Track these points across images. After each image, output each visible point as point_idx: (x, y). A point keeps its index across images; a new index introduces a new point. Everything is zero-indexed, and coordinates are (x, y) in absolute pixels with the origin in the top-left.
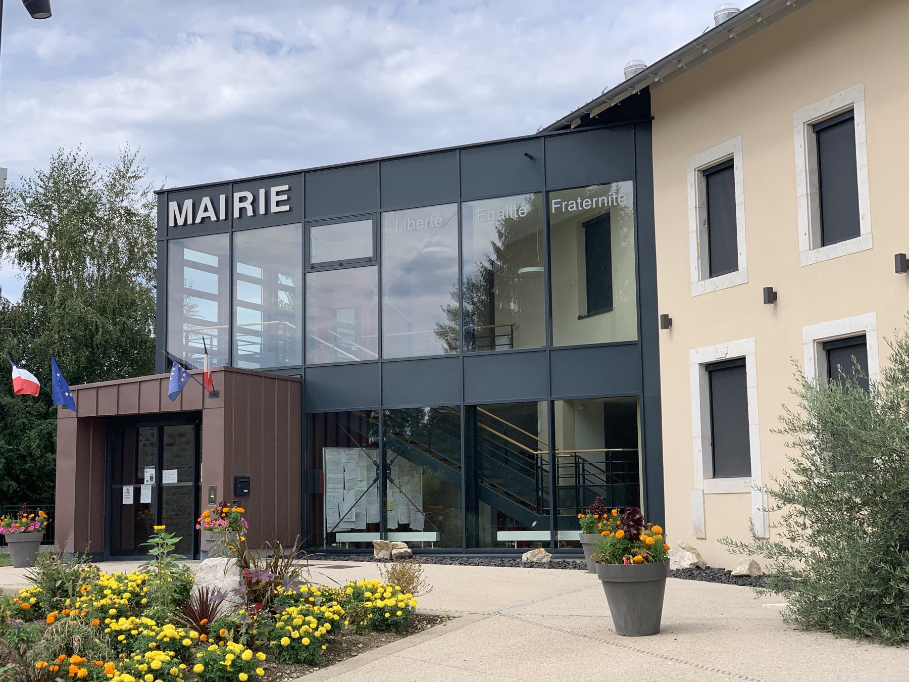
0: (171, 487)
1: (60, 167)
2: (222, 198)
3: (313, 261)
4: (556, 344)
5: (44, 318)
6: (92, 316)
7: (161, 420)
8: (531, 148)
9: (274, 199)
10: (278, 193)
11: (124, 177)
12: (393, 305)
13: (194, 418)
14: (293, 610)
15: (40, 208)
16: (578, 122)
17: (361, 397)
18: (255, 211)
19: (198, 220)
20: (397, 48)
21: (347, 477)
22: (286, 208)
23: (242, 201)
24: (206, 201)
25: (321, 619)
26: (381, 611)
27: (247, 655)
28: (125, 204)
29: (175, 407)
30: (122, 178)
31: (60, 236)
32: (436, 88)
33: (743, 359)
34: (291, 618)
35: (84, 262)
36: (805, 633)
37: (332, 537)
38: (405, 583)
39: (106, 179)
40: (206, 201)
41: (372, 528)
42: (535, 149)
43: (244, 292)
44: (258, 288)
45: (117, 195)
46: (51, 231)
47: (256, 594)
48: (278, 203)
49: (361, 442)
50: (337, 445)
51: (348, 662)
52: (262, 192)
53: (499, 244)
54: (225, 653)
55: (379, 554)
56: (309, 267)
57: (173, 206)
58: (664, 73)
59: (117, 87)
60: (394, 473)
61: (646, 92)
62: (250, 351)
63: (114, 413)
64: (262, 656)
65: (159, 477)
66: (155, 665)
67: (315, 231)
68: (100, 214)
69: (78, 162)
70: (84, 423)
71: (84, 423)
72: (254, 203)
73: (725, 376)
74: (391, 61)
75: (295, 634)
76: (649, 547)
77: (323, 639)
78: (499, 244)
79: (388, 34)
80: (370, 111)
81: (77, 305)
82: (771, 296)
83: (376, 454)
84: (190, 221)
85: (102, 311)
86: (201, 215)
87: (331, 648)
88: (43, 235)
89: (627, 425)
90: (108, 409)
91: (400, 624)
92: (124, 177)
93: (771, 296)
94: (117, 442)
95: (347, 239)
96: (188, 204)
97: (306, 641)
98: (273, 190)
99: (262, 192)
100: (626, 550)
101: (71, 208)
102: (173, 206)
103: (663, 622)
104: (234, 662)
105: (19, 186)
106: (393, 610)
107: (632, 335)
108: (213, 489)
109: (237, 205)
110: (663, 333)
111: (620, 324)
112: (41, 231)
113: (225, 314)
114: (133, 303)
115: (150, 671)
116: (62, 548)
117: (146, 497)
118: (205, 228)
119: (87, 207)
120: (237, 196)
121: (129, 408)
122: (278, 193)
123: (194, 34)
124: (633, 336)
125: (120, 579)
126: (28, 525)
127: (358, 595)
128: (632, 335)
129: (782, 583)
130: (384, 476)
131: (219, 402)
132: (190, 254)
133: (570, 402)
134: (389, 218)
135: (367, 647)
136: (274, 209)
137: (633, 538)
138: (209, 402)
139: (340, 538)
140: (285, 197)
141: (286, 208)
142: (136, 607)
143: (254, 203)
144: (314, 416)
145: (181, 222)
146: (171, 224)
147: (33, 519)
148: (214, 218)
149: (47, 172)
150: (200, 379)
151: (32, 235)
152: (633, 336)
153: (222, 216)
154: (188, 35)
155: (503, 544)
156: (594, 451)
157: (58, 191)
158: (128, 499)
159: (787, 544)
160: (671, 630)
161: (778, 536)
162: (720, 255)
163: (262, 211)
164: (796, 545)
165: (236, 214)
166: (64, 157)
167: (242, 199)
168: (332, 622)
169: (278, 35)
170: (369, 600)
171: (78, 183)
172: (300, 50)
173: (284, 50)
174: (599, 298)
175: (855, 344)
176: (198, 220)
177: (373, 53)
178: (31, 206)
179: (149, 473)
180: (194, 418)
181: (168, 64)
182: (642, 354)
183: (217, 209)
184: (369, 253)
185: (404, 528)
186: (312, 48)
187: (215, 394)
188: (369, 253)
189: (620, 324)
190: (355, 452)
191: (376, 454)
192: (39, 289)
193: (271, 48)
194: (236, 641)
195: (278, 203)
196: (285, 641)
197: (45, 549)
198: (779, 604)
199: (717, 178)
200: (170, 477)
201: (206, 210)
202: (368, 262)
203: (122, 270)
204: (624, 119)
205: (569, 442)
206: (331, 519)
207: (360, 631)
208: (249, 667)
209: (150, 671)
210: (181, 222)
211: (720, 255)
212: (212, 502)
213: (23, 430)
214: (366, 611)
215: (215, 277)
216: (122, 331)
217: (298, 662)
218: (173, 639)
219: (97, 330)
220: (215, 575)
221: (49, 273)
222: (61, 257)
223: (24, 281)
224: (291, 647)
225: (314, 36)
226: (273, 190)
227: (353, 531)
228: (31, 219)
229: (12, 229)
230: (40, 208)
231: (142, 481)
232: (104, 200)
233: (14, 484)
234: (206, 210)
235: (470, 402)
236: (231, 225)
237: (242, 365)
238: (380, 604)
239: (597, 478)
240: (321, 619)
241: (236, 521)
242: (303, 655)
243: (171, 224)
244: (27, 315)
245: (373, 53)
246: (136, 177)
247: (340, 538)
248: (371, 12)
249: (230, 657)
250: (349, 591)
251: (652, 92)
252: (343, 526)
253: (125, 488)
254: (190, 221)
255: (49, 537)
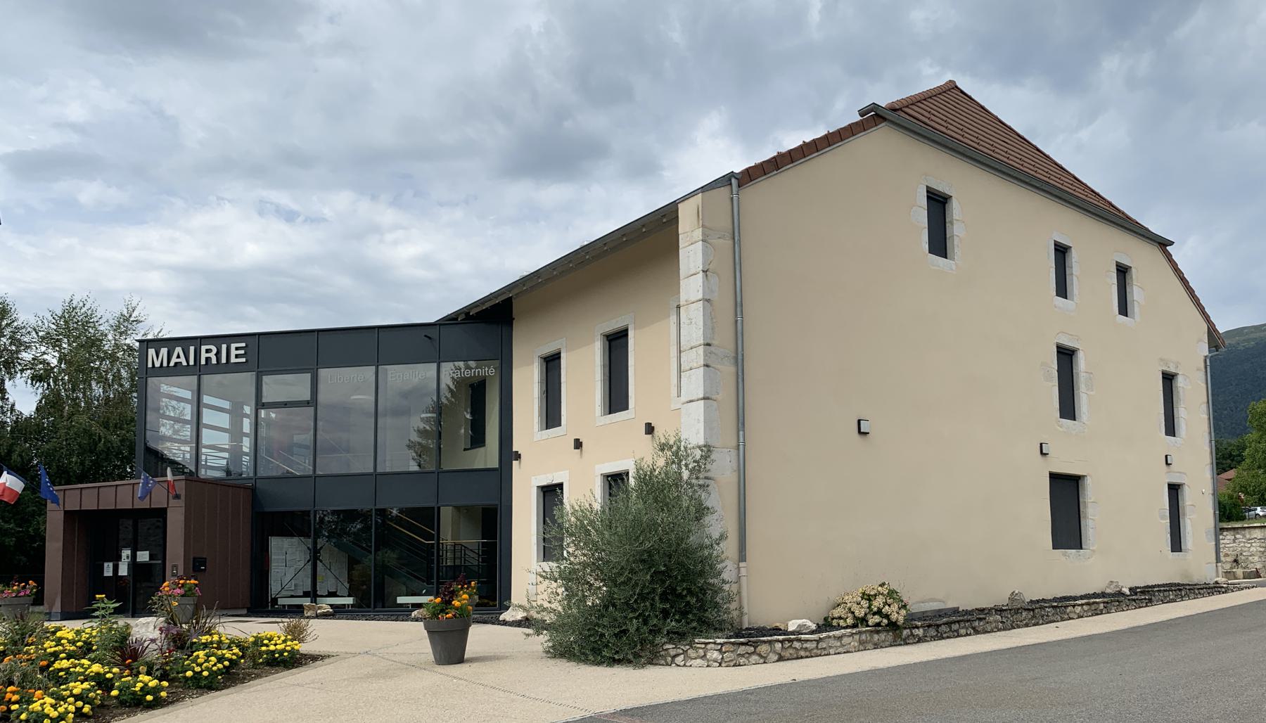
0: (144, 565)
1: (70, 310)
2: (192, 349)
3: (264, 400)
4: (445, 468)
5: (55, 427)
6: (96, 429)
7: (136, 515)
8: (429, 332)
10: (237, 349)
11: (127, 320)
13: (161, 514)
14: (201, 653)
15: (50, 340)
16: (463, 316)
17: (296, 501)
18: (218, 359)
19: (172, 364)
21: (287, 559)
22: (244, 360)
23: (208, 353)
24: (179, 350)
26: (273, 652)
27: (154, 683)
28: (128, 341)
30: (125, 323)
31: (69, 363)
32: (426, 261)
34: (198, 657)
36: (552, 662)
37: (275, 601)
38: (296, 634)
39: (111, 322)
40: (179, 350)
41: (306, 594)
42: (433, 333)
43: (208, 417)
44: (227, 416)
45: (121, 334)
46: (60, 361)
47: (180, 643)
48: (237, 356)
49: (302, 533)
51: (240, 686)
52: (224, 347)
53: (452, 387)
54: (135, 683)
56: (260, 405)
57: (152, 352)
60: (324, 555)
61: (509, 300)
62: (214, 462)
65: (134, 556)
67: (266, 379)
69: (87, 306)
72: (218, 354)
73: (551, 493)
74: (389, 237)
75: (198, 669)
76: (457, 609)
77: (219, 672)
78: (452, 387)
79: (388, 216)
80: (373, 275)
82: (578, 444)
84: (165, 364)
85: (106, 425)
86: (174, 360)
87: (229, 676)
88: (54, 362)
89: (494, 522)
90: (90, 504)
91: (293, 661)
92: (127, 320)
93: (578, 444)
96: (164, 351)
97: (205, 673)
98: (233, 346)
99: (224, 347)
100: (442, 611)
102: (152, 352)
104: (142, 689)
105: (33, 321)
106: (281, 652)
107: (494, 463)
108: (175, 566)
109: (204, 355)
111: (488, 456)
112: (52, 359)
113: (207, 432)
114: (132, 420)
115: (72, 695)
116: (51, 608)
117: (123, 571)
118: (177, 370)
119: (94, 343)
120: (204, 348)
121: (107, 504)
122: (237, 349)
123: (223, 199)
125: (78, 633)
126: (19, 592)
127: (258, 642)
128: (494, 463)
131: (181, 502)
132: (165, 388)
134: (324, 373)
135: (258, 676)
136: (233, 360)
137: (449, 602)
138: (172, 502)
139: (281, 601)
140: (242, 352)
141: (244, 360)
143: (218, 354)
145: (157, 364)
146: (150, 365)
147: (24, 587)
148: (185, 363)
149: (59, 313)
150: (165, 485)
151: (44, 362)
153: (192, 363)
155: (401, 605)
158: (108, 571)
159: (546, 605)
160: (471, 660)
161: (543, 600)
162: (551, 417)
163: (224, 361)
165: (203, 362)
167: (208, 351)
168: (230, 660)
170: (267, 645)
171: (86, 323)
172: (315, 220)
173: (301, 219)
174: (478, 439)
176: (172, 364)
177: (376, 229)
178: (43, 338)
179: (126, 553)
180: (161, 514)
181: (200, 220)
182: (501, 477)
184: (307, 397)
185: (332, 594)
186: (325, 220)
187: (177, 497)
188: (307, 397)
189: (488, 456)
190: (295, 540)
193: (289, 217)
194: (148, 673)
195: (237, 356)
196: (189, 674)
200: (143, 556)
201: (178, 357)
202: (307, 403)
203: (124, 393)
204: (493, 319)
206: (274, 588)
207: (256, 665)
209: (72, 695)
210: (157, 364)
211: (551, 417)
212: (173, 575)
213: (33, 516)
214: (261, 654)
217: (200, 687)
218: (98, 674)
220: (146, 630)
222: (69, 381)
225: (327, 212)
226: (233, 346)
228: (43, 349)
229: (27, 356)
230: (50, 340)
232: (110, 337)
233: (24, 559)
234: (178, 357)
235: (378, 507)
236: (199, 370)
237: (203, 473)
238: (272, 648)
239: (474, 560)
240: (221, 659)
243: (150, 365)
244: (38, 425)
245: (376, 229)
246: (138, 322)
247: (281, 601)
248: (374, 198)
249: (139, 685)
252: (284, 593)
253: (106, 564)
254: (165, 364)
255: (38, 599)
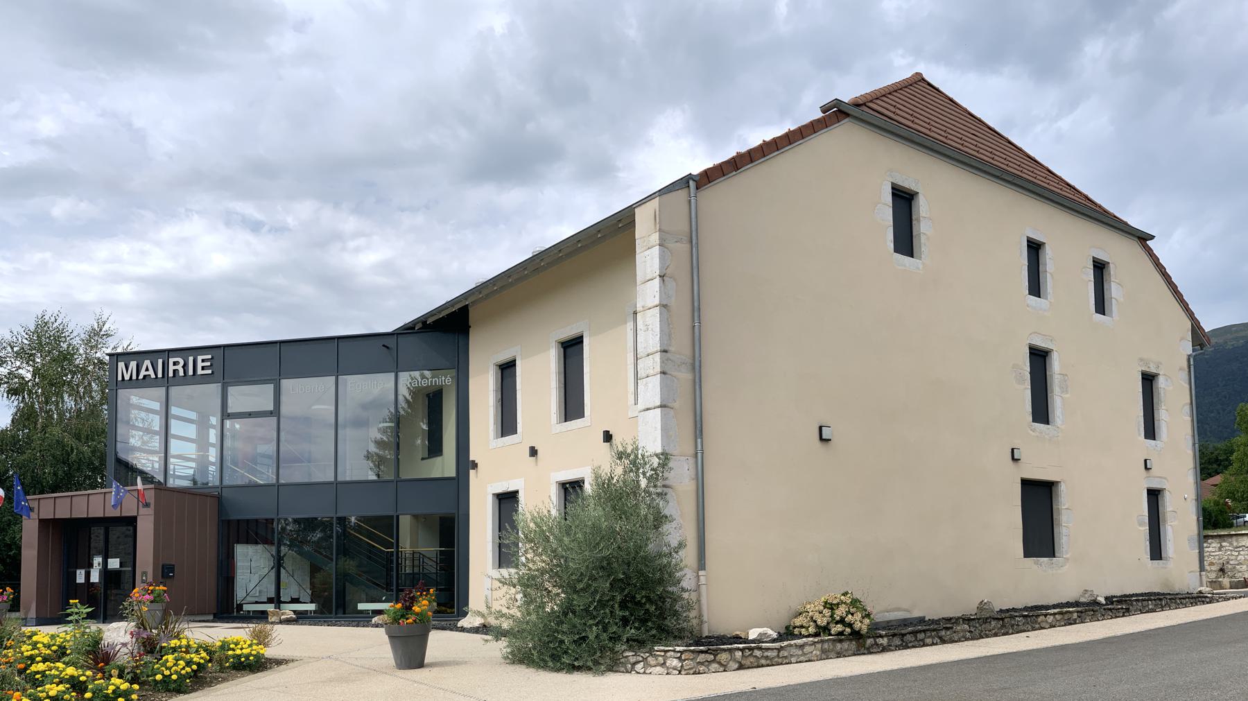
2: (160, 361)
6: (69, 440)
9: (200, 364)
12: (333, 437)
13: (132, 521)
15: (25, 355)
19: (141, 377)
20: (356, 235)
21: (252, 564)
23: (176, 365)
24: (147, 363)
25: (189, 663)
26: (239, 656)
27: (125, 686)
28: (98, 355)
29: (116, 513)
31: (43, 377)
32: (387, 267)
33: (517, 492)
34: (167, 661)
35: (62, 398)
37: (240, 607)
39: (83, 336)
40: (147, 363)
41: (270, 601)
45: (92, 347)
46: (34, 375)
47: (150, 647)
48: (203, 368)
49: (266, 541)
50: (247, 542)
53: (409, 398)
55: (272, 619)
56: (226, 415)
57: (121, 365)
58: (485, 292)
59: (123, 248)
60: (287, 563)
63: (68, 516)
64: (136, 687)
65: (105, 563)
66: (52, 693)
67: (232, 390)
68: (77, 362)
69: (59, 321)
70: (43, 522)
71: (43, 522)
73: (507, 501)
74: (352, 244)
75: (167, 673)
76: (417, 614)
77: (188, 676)
78: (409, 398)
79: (350, 223)
80: (338, 284)
81: (56, 431)
82: (534, 452)
83: (273, 549)
84: (134, 377)
85: (78, 437)
87: (198, 679)
88: (29, 376)
89: (450, 531)
90: (63, 513)
91: (257, 665)
93: (534, 452)
94: (71, 539)
95: (246, 397)
96: (133, 364)
97: (174, 677)
98: (200, 358)
99: (191, 359)
100: (403, 616)
101: (51, 358)
102: (121, 365)
103: (426, 661)
104: (114, 691)
106: (247, 657)
109: (172, 368)
110: (472, 472)
111: (445, 465)
113: (173, 442)
114: (103, 431)
116: (26, 613)
117: (95, 577)
119: (67, 357)
120: (171, 361)
123: (191, 210)
124: (453, 474)
125: (53, 637)
127: (225, 646)
129: (499, 633)
130: (278, 564)
131: (151, 511)
132: (134, 400)
133: (415, 517)
134: (285, 383)
135: (224, 680)
136: (200, 372)
137: (409, 608)
138: (143, 511)
139: (246, 607)
142: (61, 653)
144: (229, 521)
145: (127, 377)
146: (120, 378)
148: (153, 376)
150: (135, 494)
152: (453, 474)
153: (160, 375)
154: (187, 210)
155: (362, 612)
156: (430, 549)
157: (40, 343)
159: (505, 611)
160: (431, 665)
162: (507, 424)
163: (191, 372)
164: (511, 612)
165: (171, 374)
166: (47, 318)
167: (175, 364)
169: (259, 216)
171: (58, 337)
172: (279, 230)
174: (435, 448)
175: (577, 485)
176: (141, 377)
177: (337, 237)
179: (98, 560)
180: (132, 521)
181: (169, 232)
182: (458, 486)
183: (164, 369)
185: (295, 601)
186: (289, 230)
187: (147, 505)
189: (445, 465)
190: (260, 547)
191: (273, 549)
192: (24, 418)
193: (255, 227)
194: (120, 677)
195: (203, 368)
197: (14, 615)
198: (500, 647)
199: (507, 372)
200: (114, 563)
201: (147, 369)
202: (271, 413)
203: (95, 406)
204: (449, 328)
205: (412, 541)
206: (240, 594)
207: (222, 669)
208: (126, 694)
210: (127, 377)
211: (507, 424)
212: (143, 582)
213: (9, 525)
214: (227, 658)
215: (158, 417)
216: (93, 452)
217: (169, 691)
218: (72, 677)
219: (72, 450)
220: (118, 634)
221: (33, 403)
222: (43, 393)
223: (13, 410)
224: (163, 681)
225: (290, 221)
227: (257, 603)
228: (18, 363)
230: (25, 355)
231: (91, 565)
232: (81, 351)
234: (147, 369)
235: (339, 515)
236: (167, 381)
237: (171, 483)
238: (238, 652)
239: (431, 568)
240: (189, 663)
241: (159, 595)
242: (172, 686)
243: (120, 378)
244: (13, 437)
245: (337, 237)
246: (108, 335)
247: (246, 607)
248: (337, 205)
249: (111, 688)
250: (219, 644)
251: (470, 309)
252: (249, 599)
254: (134, 377)
255: (15, 606)
